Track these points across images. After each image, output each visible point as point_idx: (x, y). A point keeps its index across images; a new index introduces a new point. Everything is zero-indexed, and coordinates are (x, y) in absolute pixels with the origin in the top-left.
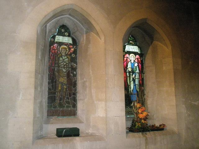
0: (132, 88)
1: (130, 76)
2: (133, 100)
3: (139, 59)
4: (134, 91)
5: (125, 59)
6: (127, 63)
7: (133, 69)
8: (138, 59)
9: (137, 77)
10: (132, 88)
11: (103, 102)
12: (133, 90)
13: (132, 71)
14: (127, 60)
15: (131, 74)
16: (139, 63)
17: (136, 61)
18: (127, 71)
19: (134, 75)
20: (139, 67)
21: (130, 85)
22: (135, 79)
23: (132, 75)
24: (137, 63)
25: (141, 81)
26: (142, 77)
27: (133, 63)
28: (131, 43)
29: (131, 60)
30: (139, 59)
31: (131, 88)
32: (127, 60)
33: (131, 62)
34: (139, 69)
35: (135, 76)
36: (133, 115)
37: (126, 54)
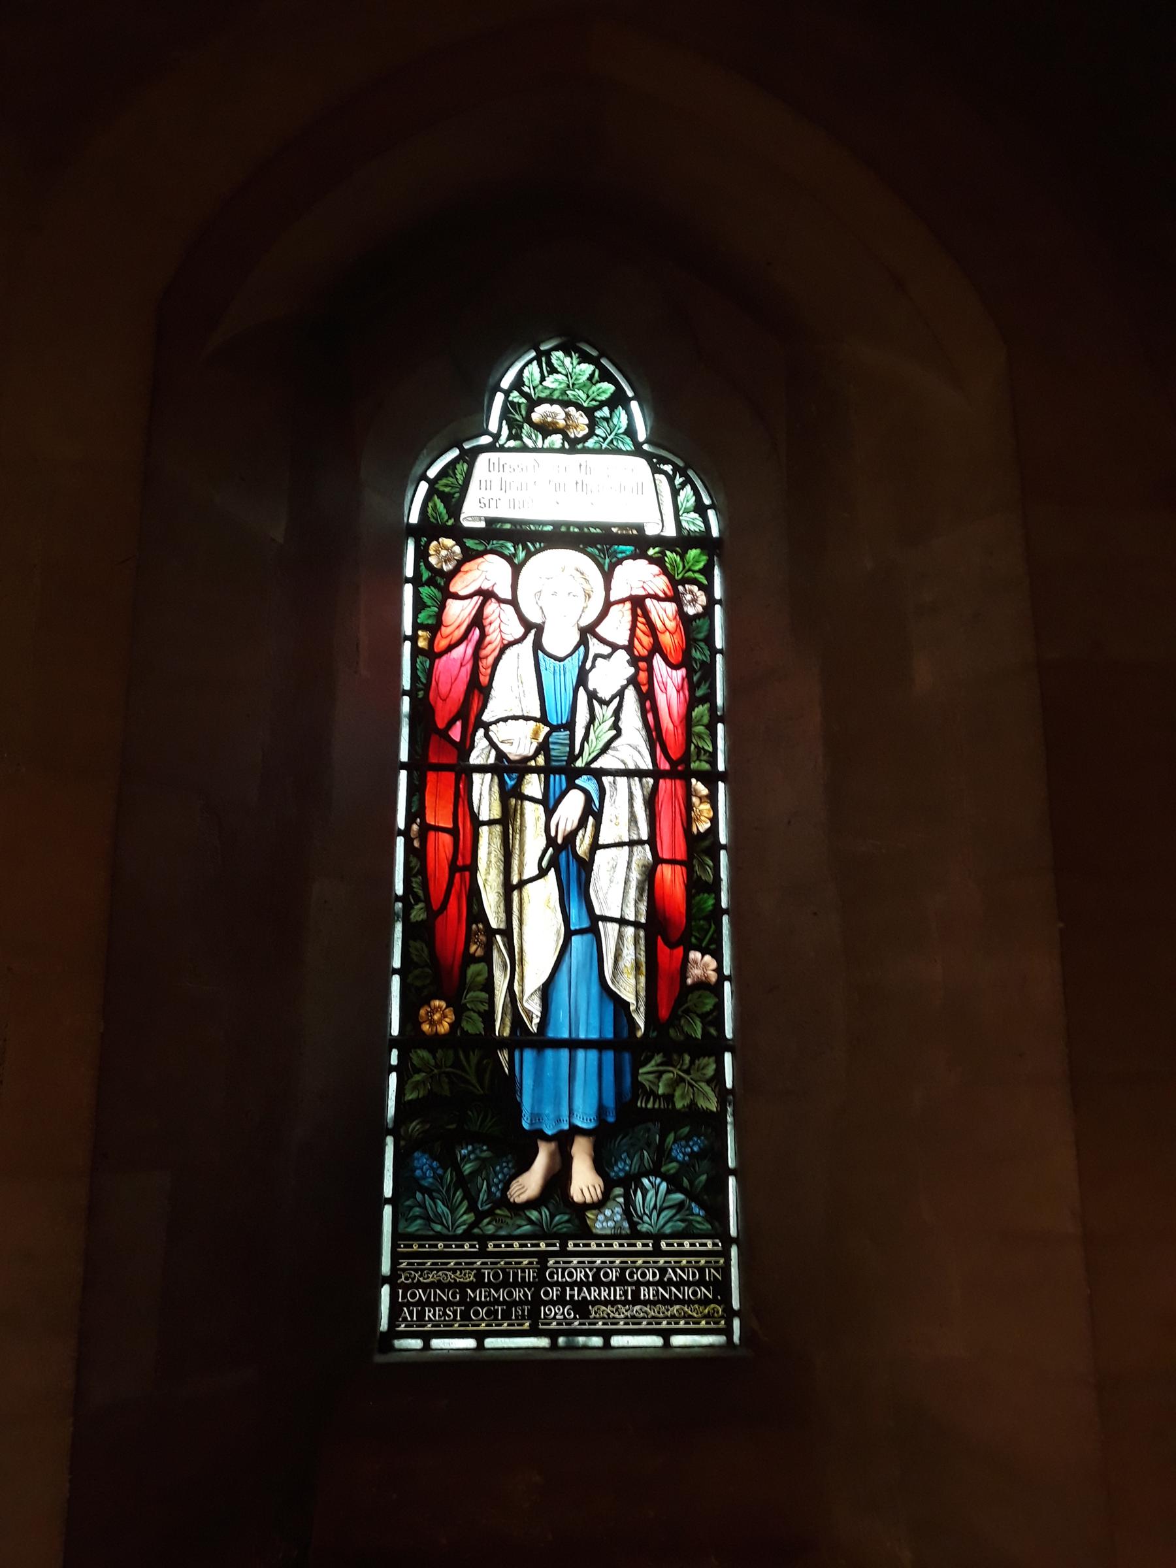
0: (536, 971)
1: (508, 820)
2: (536, 1117)
3: (663, 613)
4: (561, 995)
5: (458, 612)
6: (476, 656)
7: (570, 726)
8: (637, 603)
9: (614, 827)
10: (536, 971)
11: (450, 602)
12: (546, 991)
13: (544, 747)
14: (478, 621)
15: (533, 786)
16: (657, 647)
17: (617, 626)
18: (475, 758)
19: (571, 808)
20: (647, 699)
21: (507, 933)
22: (582, 846)
23: (550, 806)
24: (622, 656)
25: (671, 877)
26: (688, 821)
27: (573, 665)
28: (545, 429)
29: (511, 1218)
30: (663, 613)
31: (515, 962)
32: (478, 621)
33: (538, 646)
34: (654, 735)
35: (592, 812)
36: (534, 1332)
37: (469, 556)
